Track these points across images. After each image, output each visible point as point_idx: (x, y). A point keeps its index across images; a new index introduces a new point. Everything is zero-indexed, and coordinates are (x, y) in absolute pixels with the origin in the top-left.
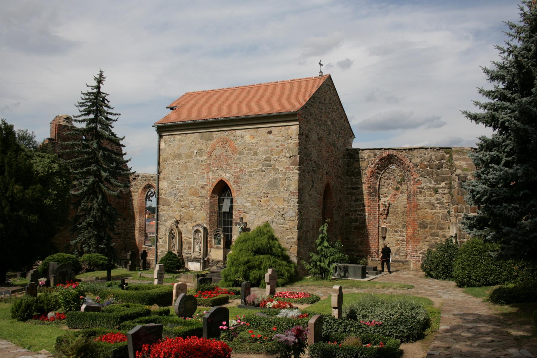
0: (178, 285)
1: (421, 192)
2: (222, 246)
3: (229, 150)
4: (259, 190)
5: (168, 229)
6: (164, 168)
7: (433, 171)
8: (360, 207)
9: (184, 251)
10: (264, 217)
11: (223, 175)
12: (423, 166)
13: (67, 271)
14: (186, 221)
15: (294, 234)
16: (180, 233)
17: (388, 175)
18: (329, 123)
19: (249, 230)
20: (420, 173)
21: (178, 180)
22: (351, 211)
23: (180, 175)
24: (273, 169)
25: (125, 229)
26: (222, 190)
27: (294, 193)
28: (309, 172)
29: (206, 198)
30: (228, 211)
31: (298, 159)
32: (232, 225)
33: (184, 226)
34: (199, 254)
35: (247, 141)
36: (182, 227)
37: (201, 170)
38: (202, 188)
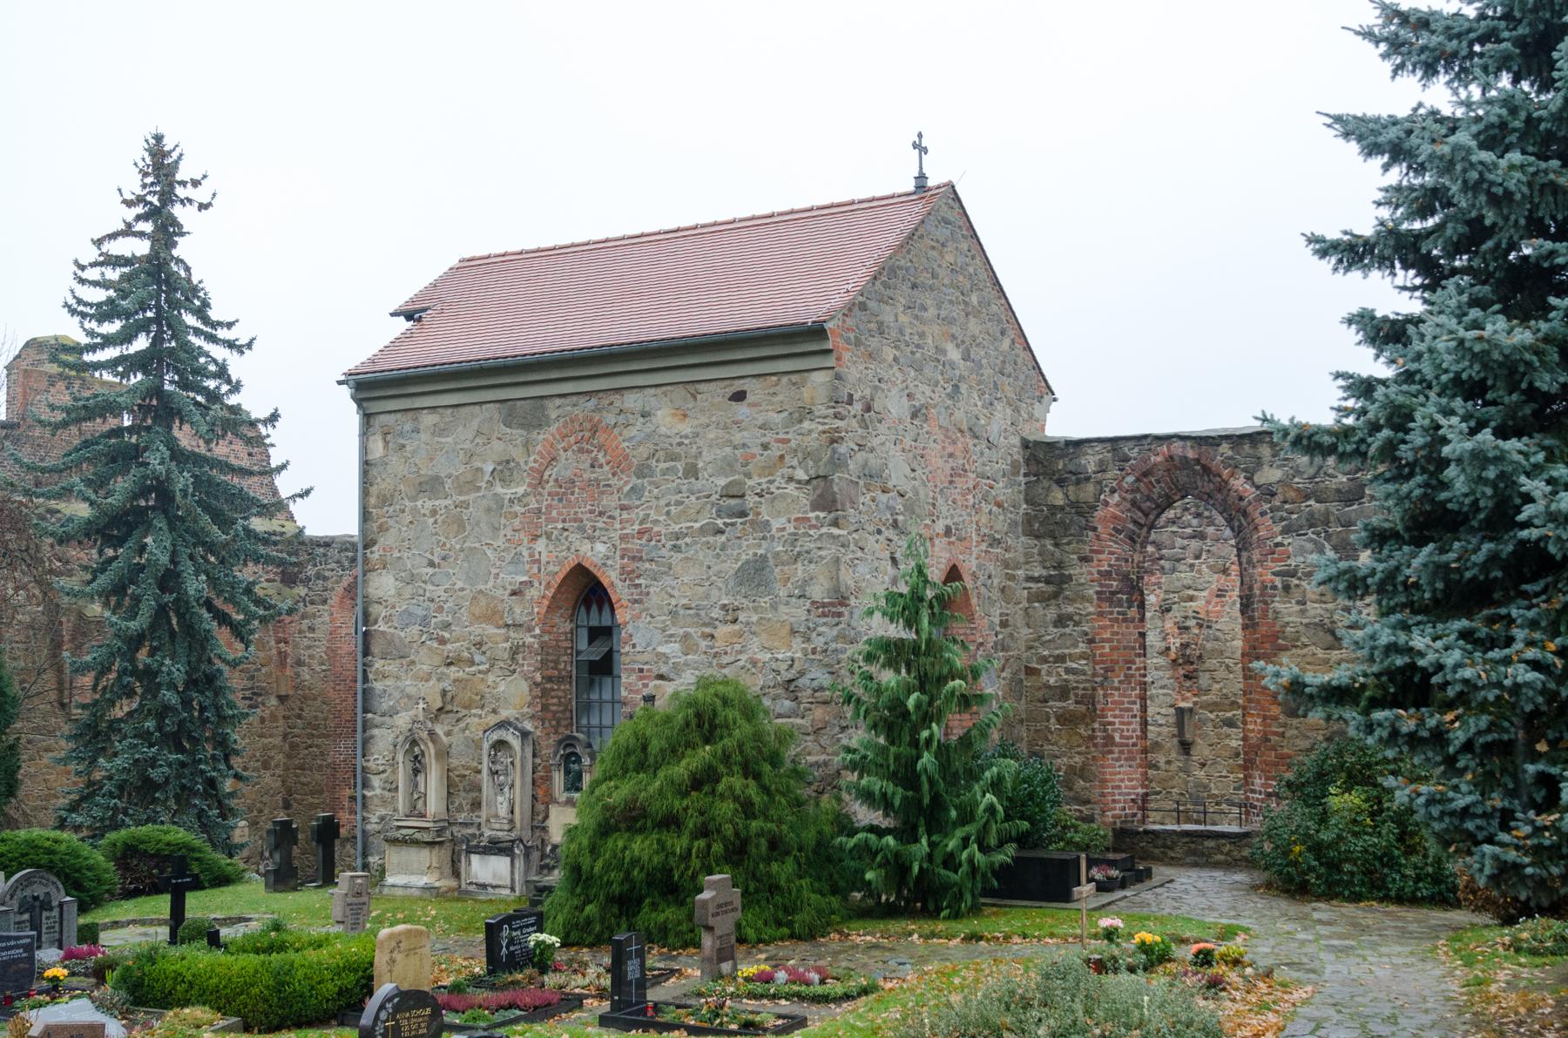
1: (1287, 588)
3: (602, 460)
4: (707, 596)
5: (401, 738)
6: (383, 529)
7: (1327, 513)
8: (1075, 645)
11: (585, 547)
12: (1292, 494)
14: (464, 712)
17: (1195, 522)
18: (954, 354)
20: (1282, 519)
21: (430, 571)
22: (1044, 660)
24: (752, 522)
25: (285, 736)
27: (824, 605)
28: (879, 532)
29: (530, 630)
33: (456, 729)
35: (663, 430)
37: (509, 533)
38: (514, 593)
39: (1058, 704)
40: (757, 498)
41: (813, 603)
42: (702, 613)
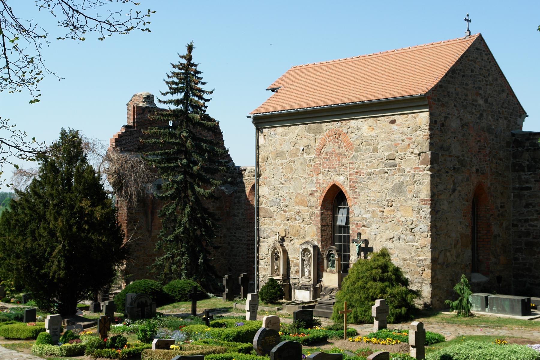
0: (268, 319)
2: (336, 269)
3: (343, 146)
4: (381, 197)
5: (270, 247)
8: (533, 215)
9: (292, 276)
10: (388, 232)
13: (146, 301)
15: (427, 255)
16: (285, 252)
18: (481, 102)
19: (371, 250)
21: (281, 186)
22: (520, 221)
23: (283, 178)
25: (229, 243)
26: (335, 198)
27: (425, 200)
29: (316, 208)
30: (344, 224)
31: (430, 157)
32: (349, 242)
34: (308, 280)
35: (365, 134)
36: (287, 245)
37: (309, 172)
38: (311, 194)
39: (525, 238)
40: (400, 160)
41: (421, 199)
42: (379, 203)
